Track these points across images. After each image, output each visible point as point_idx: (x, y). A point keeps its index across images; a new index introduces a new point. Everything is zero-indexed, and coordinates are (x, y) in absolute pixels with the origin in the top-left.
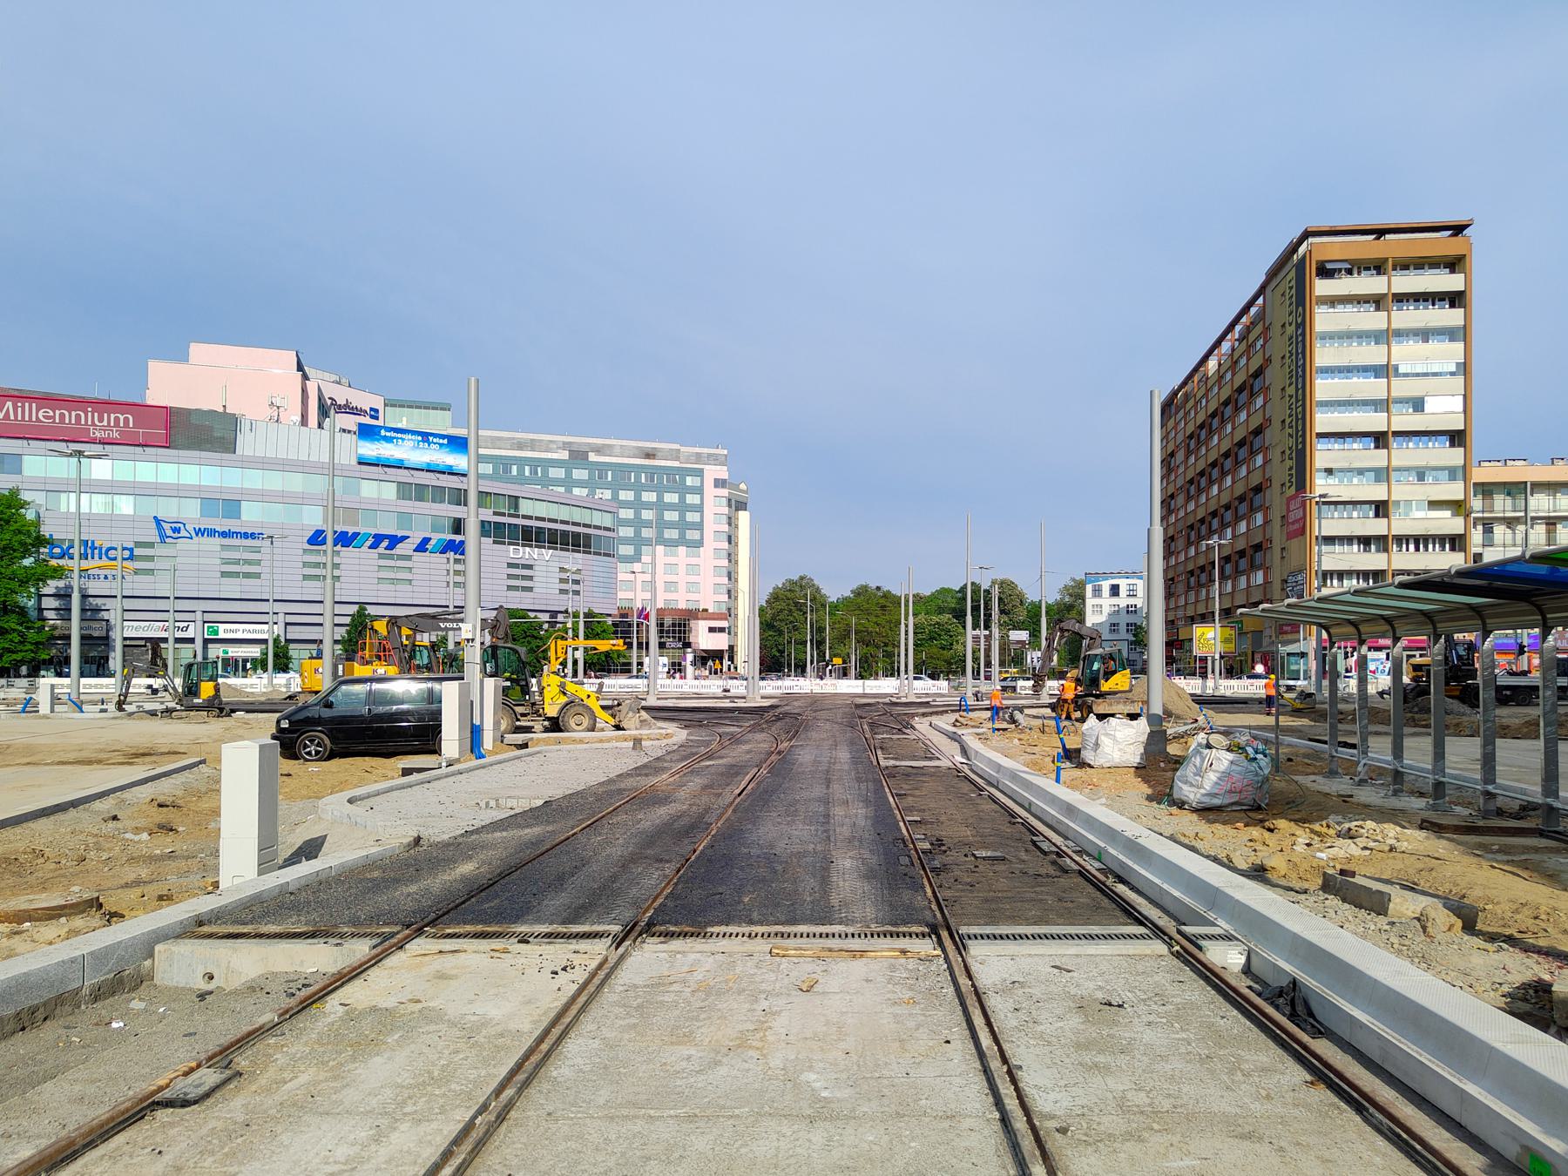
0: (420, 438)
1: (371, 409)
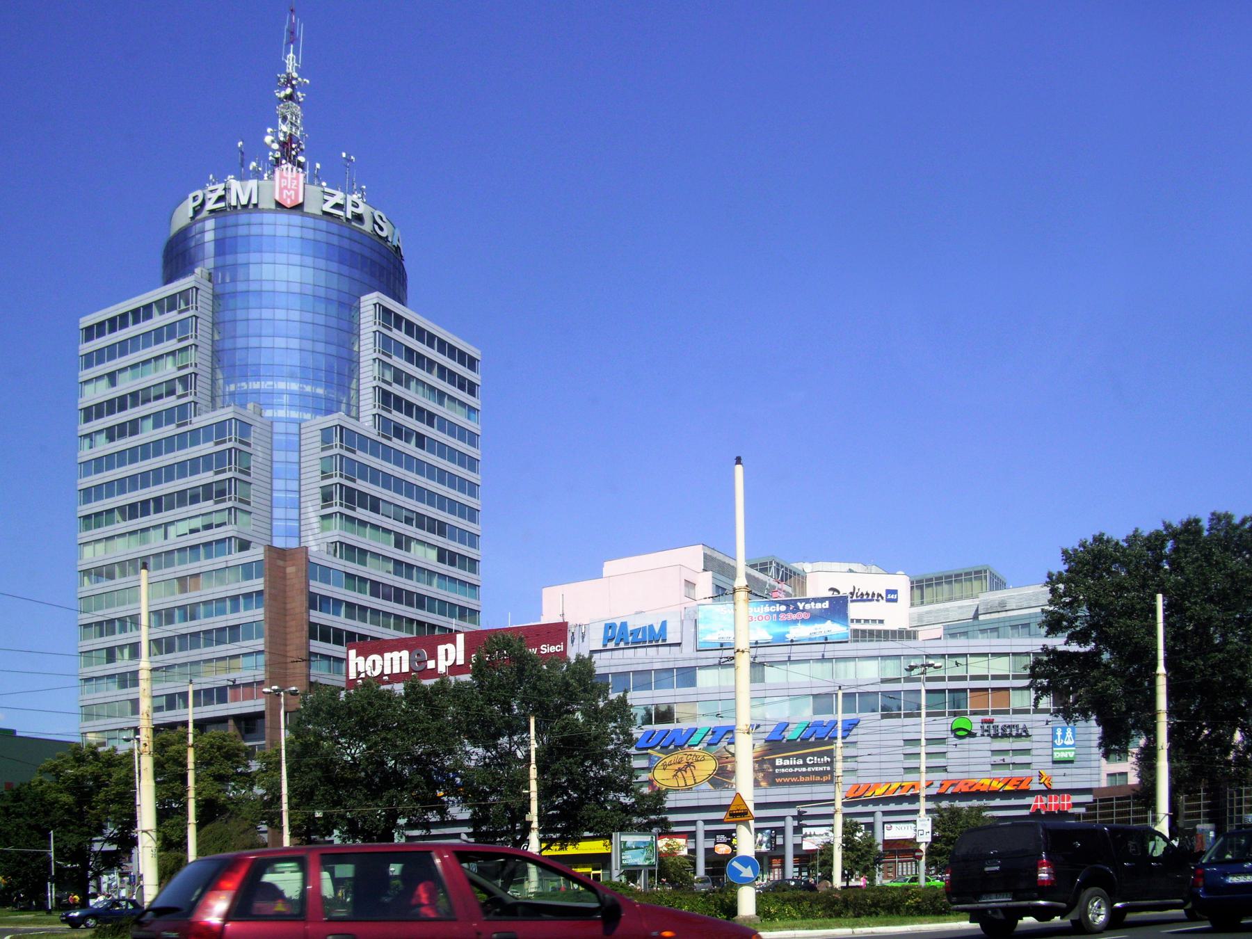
0: (783, 608)
1: (888, 592)
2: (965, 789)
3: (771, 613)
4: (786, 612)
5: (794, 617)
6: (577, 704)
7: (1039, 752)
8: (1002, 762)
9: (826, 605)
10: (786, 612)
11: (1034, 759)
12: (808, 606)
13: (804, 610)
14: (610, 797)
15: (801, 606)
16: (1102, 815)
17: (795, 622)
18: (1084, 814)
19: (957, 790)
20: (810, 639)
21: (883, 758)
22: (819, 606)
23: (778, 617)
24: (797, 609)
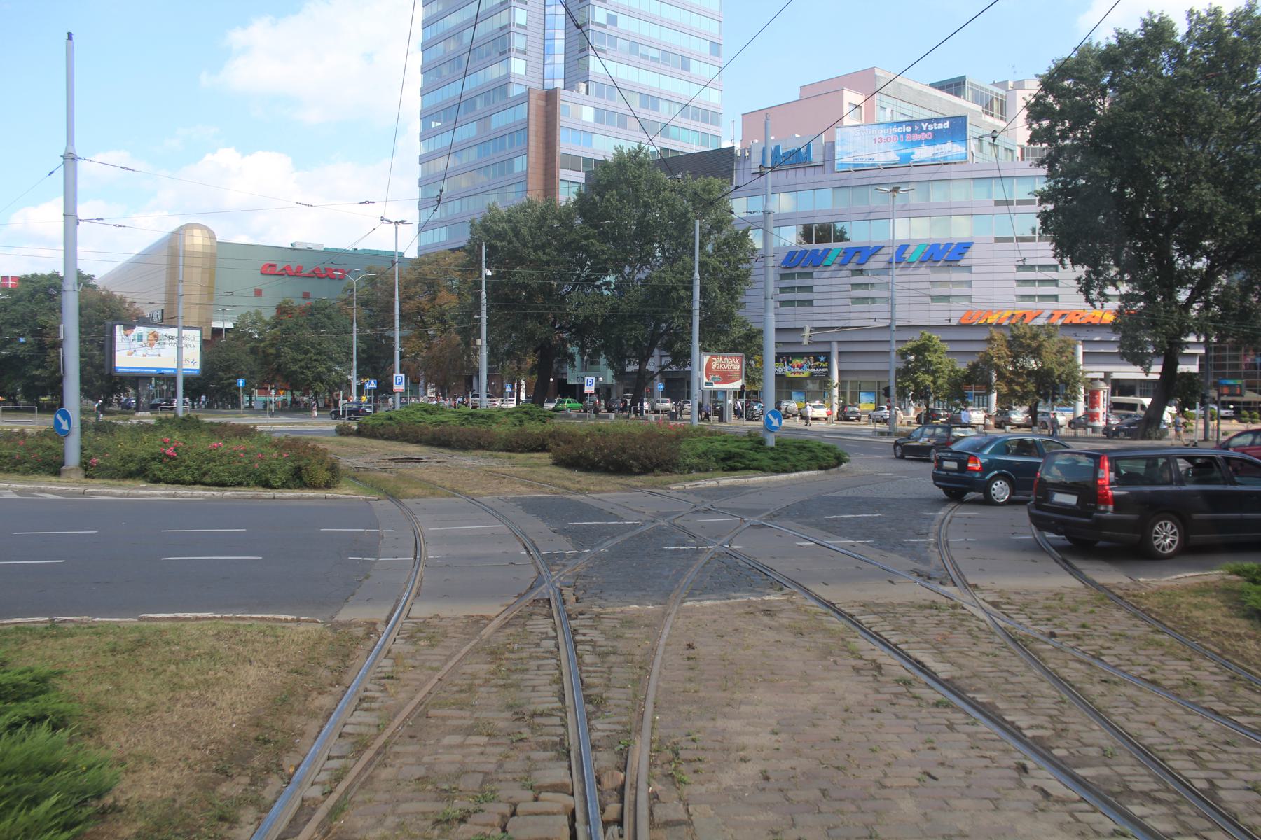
0: (909, 129)
2: (1076, 321)
3: (898, 134)
4: (911, 133)
5: (917, 137)
6: (1157, 280)
7: (546, 694)
8: (947, 323)
9: (947, 125)
10: (911, 133)
11: (974, 292)
12: (931, 127)
13: (927, 130)
14: (50, 644)
15: (924, 126)
16: (1224, 358)
17: (918, 143)
18: (1225, 378)
19: (1067, 321)
20: (933, 160)
21: (867, 315)
22: (940, 126)
23: (904, 138)
24: (921, 131)
